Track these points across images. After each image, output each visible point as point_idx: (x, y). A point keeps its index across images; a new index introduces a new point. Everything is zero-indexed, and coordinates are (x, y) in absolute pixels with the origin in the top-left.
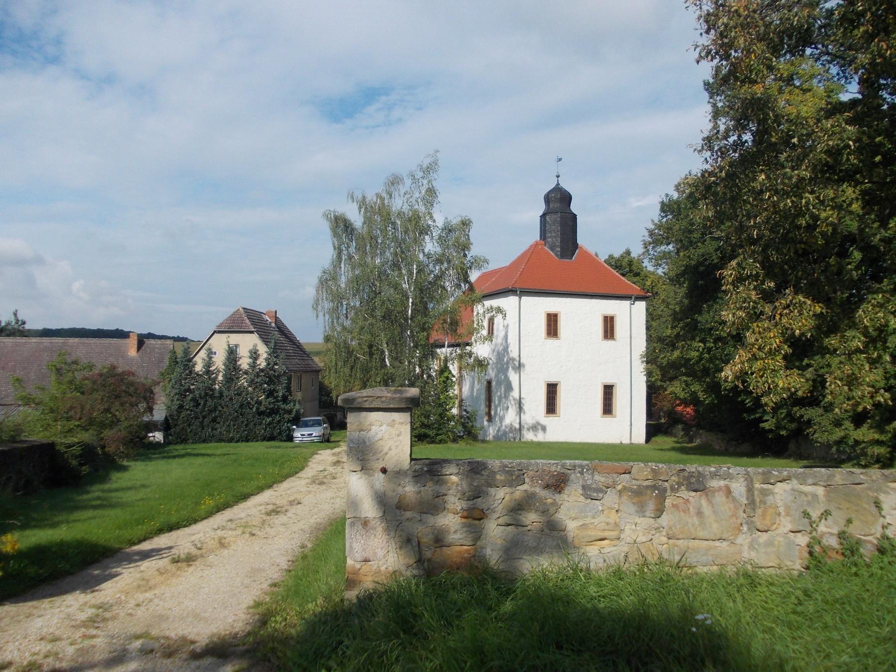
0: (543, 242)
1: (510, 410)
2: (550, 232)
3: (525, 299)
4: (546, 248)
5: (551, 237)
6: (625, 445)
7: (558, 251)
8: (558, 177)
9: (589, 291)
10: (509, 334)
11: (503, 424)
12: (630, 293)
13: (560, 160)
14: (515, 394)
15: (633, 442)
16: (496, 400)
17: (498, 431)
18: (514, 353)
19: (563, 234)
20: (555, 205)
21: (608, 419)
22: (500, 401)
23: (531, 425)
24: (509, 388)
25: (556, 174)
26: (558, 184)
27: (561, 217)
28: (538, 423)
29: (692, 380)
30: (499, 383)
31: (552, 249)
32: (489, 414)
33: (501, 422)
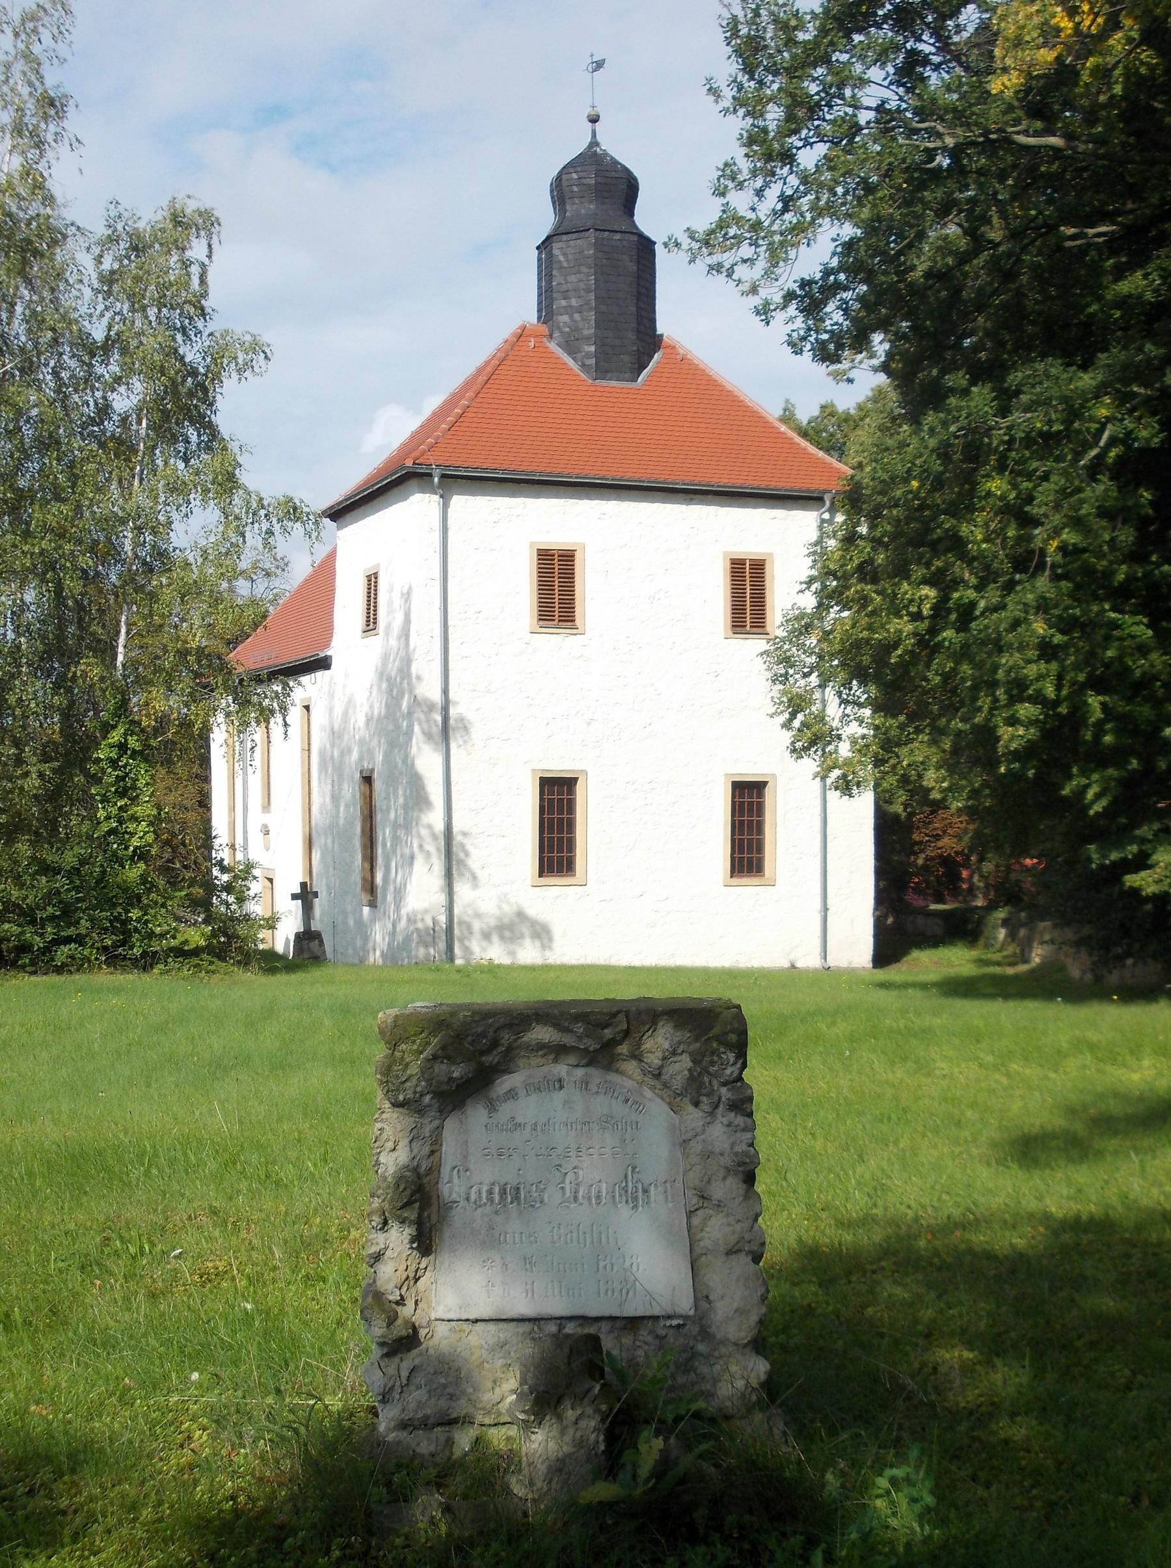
0: (544, 329)
1: (419, 864)
2: (565, 295)
3: (462, 504)
4: (553, 346)
5: (569, 310)
6: (807, 971)
7: (588, 355)
8: (594, 120)
9: (680, 479)
10: (413, 617)
11: (404, 912)
12: (815, 484)
13: (599, 65)
14: (435, 818)
15: (832, 961)
16: (384, 834)
17: (393, 934)
18: (431, 690)
19: (604, 297)
20: (583, 209)
21: (747, 891)
22: (396, 839)
23: (493, 922)
24: (418, 798)
25: (588, 111)
26: (594, 143)
27: (598, 245)
28: (521, 915)
29: (902, 727)
30: (392, 779)
31: (571, 347)
32: (370, 887)
33: (398, 908)
